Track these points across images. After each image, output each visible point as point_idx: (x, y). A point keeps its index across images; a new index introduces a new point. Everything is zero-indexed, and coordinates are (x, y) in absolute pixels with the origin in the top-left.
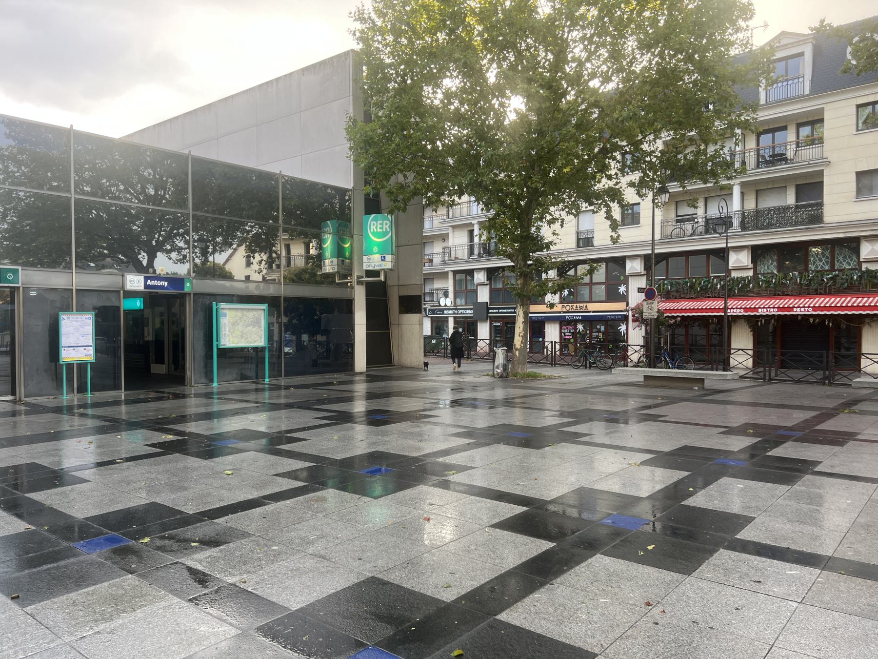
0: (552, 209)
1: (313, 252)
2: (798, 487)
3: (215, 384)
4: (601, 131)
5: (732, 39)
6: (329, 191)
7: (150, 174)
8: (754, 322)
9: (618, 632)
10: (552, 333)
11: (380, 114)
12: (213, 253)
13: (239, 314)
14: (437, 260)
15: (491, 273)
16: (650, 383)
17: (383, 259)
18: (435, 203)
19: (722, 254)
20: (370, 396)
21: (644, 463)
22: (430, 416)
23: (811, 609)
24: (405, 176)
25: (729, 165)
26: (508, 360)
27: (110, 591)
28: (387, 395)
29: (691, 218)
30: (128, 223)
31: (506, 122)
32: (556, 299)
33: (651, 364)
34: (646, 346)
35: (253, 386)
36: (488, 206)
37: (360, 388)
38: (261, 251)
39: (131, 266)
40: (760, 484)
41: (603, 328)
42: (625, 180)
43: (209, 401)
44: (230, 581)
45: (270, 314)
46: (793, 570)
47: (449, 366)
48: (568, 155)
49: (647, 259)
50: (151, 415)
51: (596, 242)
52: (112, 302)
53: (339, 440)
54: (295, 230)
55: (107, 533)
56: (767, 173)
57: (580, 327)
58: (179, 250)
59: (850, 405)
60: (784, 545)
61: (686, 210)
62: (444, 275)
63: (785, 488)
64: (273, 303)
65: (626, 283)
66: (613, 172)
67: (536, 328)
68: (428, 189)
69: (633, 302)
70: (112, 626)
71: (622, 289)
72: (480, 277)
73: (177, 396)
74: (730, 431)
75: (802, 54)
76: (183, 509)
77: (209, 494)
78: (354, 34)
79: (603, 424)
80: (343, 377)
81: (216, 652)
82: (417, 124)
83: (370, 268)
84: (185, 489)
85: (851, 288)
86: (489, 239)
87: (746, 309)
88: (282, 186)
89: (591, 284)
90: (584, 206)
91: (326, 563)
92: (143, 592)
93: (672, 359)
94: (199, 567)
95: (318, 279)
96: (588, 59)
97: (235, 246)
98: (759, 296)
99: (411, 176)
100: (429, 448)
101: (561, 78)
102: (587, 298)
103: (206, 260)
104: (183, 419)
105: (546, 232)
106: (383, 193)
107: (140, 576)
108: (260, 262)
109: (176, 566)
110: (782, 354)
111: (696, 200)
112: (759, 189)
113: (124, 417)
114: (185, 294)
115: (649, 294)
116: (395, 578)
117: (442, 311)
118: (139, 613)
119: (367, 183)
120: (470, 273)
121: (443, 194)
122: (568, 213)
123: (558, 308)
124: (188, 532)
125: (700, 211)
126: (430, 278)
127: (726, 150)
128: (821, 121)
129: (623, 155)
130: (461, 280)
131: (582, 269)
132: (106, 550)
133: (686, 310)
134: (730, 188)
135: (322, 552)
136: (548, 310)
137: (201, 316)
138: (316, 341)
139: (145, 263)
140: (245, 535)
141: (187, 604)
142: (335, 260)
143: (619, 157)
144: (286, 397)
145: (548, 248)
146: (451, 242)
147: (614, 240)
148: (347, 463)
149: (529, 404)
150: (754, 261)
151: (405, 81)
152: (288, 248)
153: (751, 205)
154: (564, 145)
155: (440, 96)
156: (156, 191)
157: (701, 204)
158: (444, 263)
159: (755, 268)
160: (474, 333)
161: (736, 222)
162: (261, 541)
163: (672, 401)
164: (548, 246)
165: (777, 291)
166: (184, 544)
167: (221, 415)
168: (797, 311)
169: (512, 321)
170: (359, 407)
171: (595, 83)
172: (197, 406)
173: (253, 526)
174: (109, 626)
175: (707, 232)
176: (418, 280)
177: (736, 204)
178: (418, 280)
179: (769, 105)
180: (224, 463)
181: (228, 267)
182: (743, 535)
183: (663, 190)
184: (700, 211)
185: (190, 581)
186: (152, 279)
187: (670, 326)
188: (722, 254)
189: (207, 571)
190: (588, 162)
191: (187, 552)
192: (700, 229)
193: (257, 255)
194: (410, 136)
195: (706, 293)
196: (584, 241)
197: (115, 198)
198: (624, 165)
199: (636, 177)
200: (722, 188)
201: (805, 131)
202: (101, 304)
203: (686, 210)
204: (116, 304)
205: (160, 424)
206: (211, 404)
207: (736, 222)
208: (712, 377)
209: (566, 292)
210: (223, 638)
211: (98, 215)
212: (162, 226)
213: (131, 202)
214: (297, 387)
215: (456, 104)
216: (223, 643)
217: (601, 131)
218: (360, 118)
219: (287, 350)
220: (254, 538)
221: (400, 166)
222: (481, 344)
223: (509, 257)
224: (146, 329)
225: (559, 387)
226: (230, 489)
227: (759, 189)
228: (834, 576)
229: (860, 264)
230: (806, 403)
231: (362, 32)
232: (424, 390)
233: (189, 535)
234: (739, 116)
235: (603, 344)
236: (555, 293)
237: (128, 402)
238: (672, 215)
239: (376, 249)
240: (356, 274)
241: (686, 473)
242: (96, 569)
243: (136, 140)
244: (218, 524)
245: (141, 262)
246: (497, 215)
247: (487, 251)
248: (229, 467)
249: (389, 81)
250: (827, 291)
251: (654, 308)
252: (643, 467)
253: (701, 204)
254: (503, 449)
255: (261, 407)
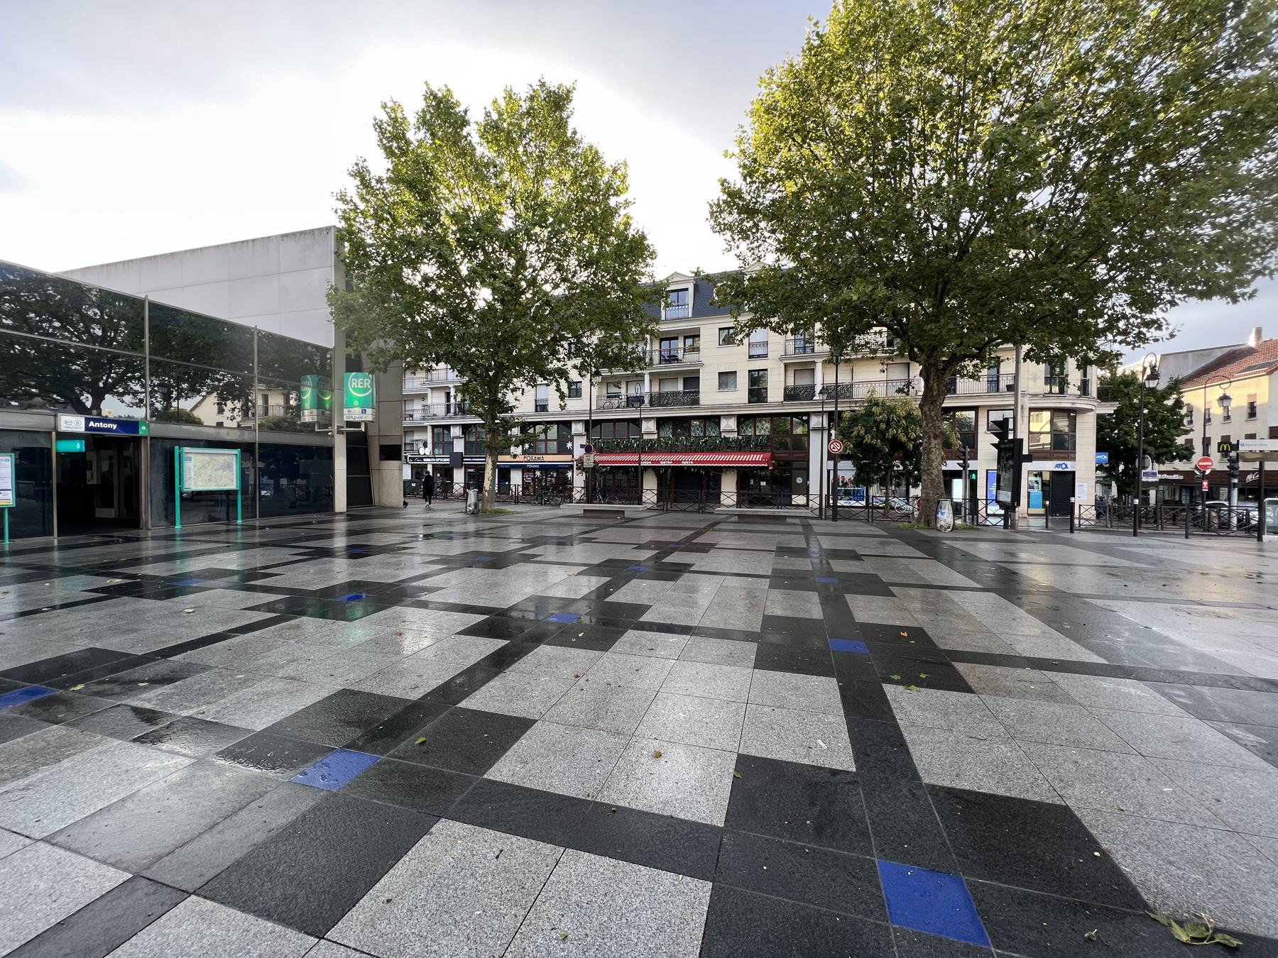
0: (515, 380)
1: (292, 402)
2: (680, 582)
3: (178, 527)
4: (551, 324)
5: (643, 270)
6: (310, 348)
7: (96, 314)
8: (657, 471)
9: (554, 701)
10: (516, 478)
11: (361, 286)
12: (178, 398)
13: (207, 458)
14: (417, 415)
15: (465, 428)
16: (588, 515)
17: (364, 412)
18: (414, 367)
19: (637, 422)
20: (350, 533)
21: (579, 574)
22: (405, 548)
23: (683, 663)
24: (385, 342)
25: (641, 359)
26: (479, 499)
27: (26, 745)
28: (367, 531)
29: (617, 396)
30: (67, 362)
31: (476, 308)
32: (518, 451)
33: (588, 502)
34: (586, 487)
35: (224, 528)
36: (461, 373)
37: (341, 526)
38: (233, 400)
39: (69, 407)
40: (657, 582)
41: (555, 475)
42: (570, 363)
43: (170, 543)
44: (184, 715)
45: (243, 459)
46: (673, 638)
47: (422, 504)
48: (526, 340)
49: (586, 422)
50: (94, 560)
51: (550, 409)
52: (43, 443)
53: (316, 573)
54: (273, 382)
55: (24, 686)
56: (666, 368)
57: (538, 473)
58: (135, 393)
59: (712, 526)
60: (669, 622)
61: (614, 390)
62: (424, 429)
63: (672, 583)
64: (246, 449)
65: (572, 441)
66: (561, 356)
67: (504, 474)
68: (408, 355)
69: (577, 457)
70: (27, 782)
71: (569, 445)
72: (456, 432)
73: (128, 540)
74: (640, 547)
75: (687, 289)
76: (130, 652)
77: (164, 634)
78: (336, 212)
79: (554, 547)
80: (322, 517)
81: (165, 785)
82: (397, 298)
83: (351, 420)
84: (134, 631)
85: (715, 449)
86: (463, 400)
87: (653, 462)
88: (258, 340)
89: (546, 440)
90: (540, 380)
91: (296, 684)
92: (72, 741)
93: (604, 497)
94: (148, 706)
95: (299, 427)
96: (542, 268)
97: (204, 394)
98: (661, 452)
99: (391, 342)
100: (404, 575)
101: (521, 279)
102: (543, 451)
103: (169, 405)
104: (137, 561)
105: (510, 398)
106: (364, 355)
107: (69, 724)
108: (233, 410)
109: (120, 708)
110: (675, 493)
111: (620, 383)
112: (660, 378)
113: (57, 563)
114: (140, 438)
115: (588, 449)
116: (365, 688)
117: (422, 459)
118: (66, 763)
119: (348, 345)
120: (447, 427)
121: (422, 360)
122: (528, 384)
123: (521, 458)
124: (137, 673)
125: (623, 391)
126: (410, 430)
127: (640, 349)
128: (699, 336)
129: (570, 344)
130: (438, 434)
131: (539, 428)
132: (23, 703)
133: (613, 462)
134: (643, 375)
135: (292, 674)
136: (512, 459)
137: (160, 460)
138: (295, 485)
139: (89, 404)
140: (205, 668)
141: (132, 744)
142: (315, 411)
143: (566, 346)
144: (260, 536)
145: (512, 411)
146: (429, 401)
147: (562, 408)
148: (327, 592)
149: (497, 535)
150: (658, 428)
151: (386, 261)
152: (266, 398)
153: (656, 389)
154: (523, 332)
155: (419, 278)
156: (104, 332)
157: (623, 386)
158: (424, 418)
159: (658, 433)
160: (451, 478)
161: (647, 400)
162: (224, 672)
163: (602, 527)
164: (511, 409)
165: (672, 450)
166: (131, 686)
167: (184, 556)
168: (684, 464)
169: (481, 469)
170: (340, 542)
171: (547, 288)
172: (154, 548)
173: (216, 658)
174: (22, 782)
175: (628, 406)
176: (399, 432)
177: (646, 388)
178: (399, 432)
179: (667, 321)
180: (186, 603)
181: (196, 413)
182: (646, 618)
183: (597, 373)
184: (623, 391)
185: (136, 721)
186: (95, 420)
187: (603, 473)
188: (637, 422)
189: (157, 708)
190: (543, 346)
191: (134, 692)
192: (623, 404)
193: (229, 403)
194: (391, 308)
195: (627, 449)
196: (541, 407)
197: (47, 335)
198: (570, 352)
199: (578, 361)
200: (637, 375)
201: (689, 342)
202: (23, 445)
203: (614, 390)
204: (46, 445)
205: (105, 568)
206: (173, 546)
207: (647, 400)
208: (630, 509)
209: (527, 446)
210: (173, 770)
211: (23, 351)
212: (111, 368)
213: (70, 339)
214: (272, 527)
215: (433, 287)
216: (174, 776)
217: (551, 324)
218: (342, 287)
219: (263, 493)
220: (216, 670)
221: (381, 333)
222: (456, 487)
223: (480, 415)
224: (88, 473)
225: (520, 520)
226: (190, 627)
227: (660, 378)
228: (698, 639)
229: (720, 433)
230: (688, 525)
231: (344, 211)
232: (403, 527)
233: (137, 676)
234: (647, 326)
235: (555, 487)
236: (517, 446)
237: (61, 548)
238: (604, 392)
239: (356, 403)
240: (336, 424)
241: (608, 579)
242: (7, 725)
243: (77, 278)
244: (173, 662)
245: (84, 404)
246: (470, 381)
247: (462, 411)
248: (189, 606)
249: (371, 258)
250: (701, 450)
251: (590, 461)
252: (579, 577)
253: (623, 386)
254: (476, 571)
255: (230, 546)
